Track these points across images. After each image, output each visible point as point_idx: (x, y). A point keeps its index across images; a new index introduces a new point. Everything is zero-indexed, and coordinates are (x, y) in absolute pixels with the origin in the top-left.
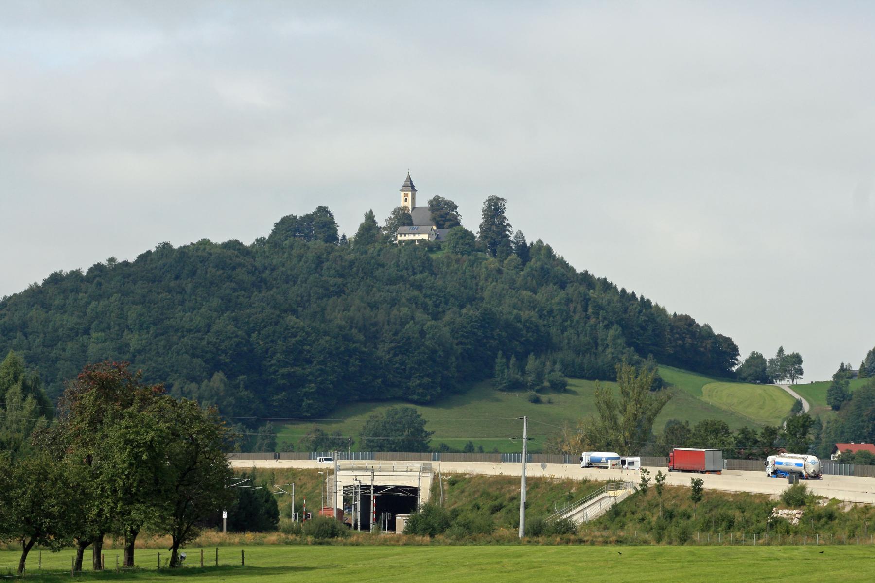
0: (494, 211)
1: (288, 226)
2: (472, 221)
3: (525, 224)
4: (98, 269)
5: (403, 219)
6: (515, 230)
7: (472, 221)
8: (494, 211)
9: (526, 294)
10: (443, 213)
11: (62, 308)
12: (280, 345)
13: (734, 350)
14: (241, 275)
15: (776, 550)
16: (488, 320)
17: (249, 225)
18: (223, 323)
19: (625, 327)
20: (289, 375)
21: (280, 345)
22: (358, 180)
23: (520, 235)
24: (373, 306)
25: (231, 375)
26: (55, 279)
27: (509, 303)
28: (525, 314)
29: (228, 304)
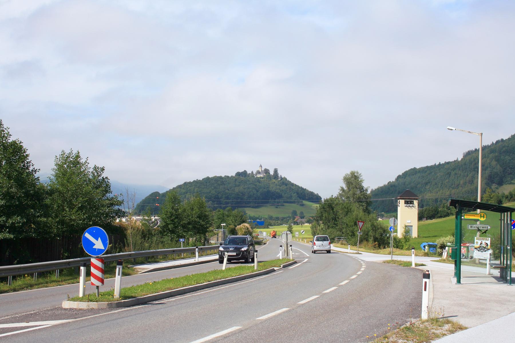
0: (276, 171)
1: (238, 174)
2: (272, 173)
3: (282, 173)
4: (194, 181)
5: (258, 172)
6: (91, 166)
7: (272, 173)
8: (276, 171)
9: (278, 187)
10: (267, 171)
11: (184, 189)
12: (224, 196)
13: (321, 198)
14: (219, 182)
15: (210, 270)
16: (269, 192)
17: (231, 173)
18: (213, 192)
19: (298, 193)
20: (226, 202)
21: (224, 196)
22: (252, 166)
23: (281, 176)
24: (245, 189)
25: (213, 202)
26: (185, 183)
27: (273, 188)
28: (277, 191)
29: (215, 188)
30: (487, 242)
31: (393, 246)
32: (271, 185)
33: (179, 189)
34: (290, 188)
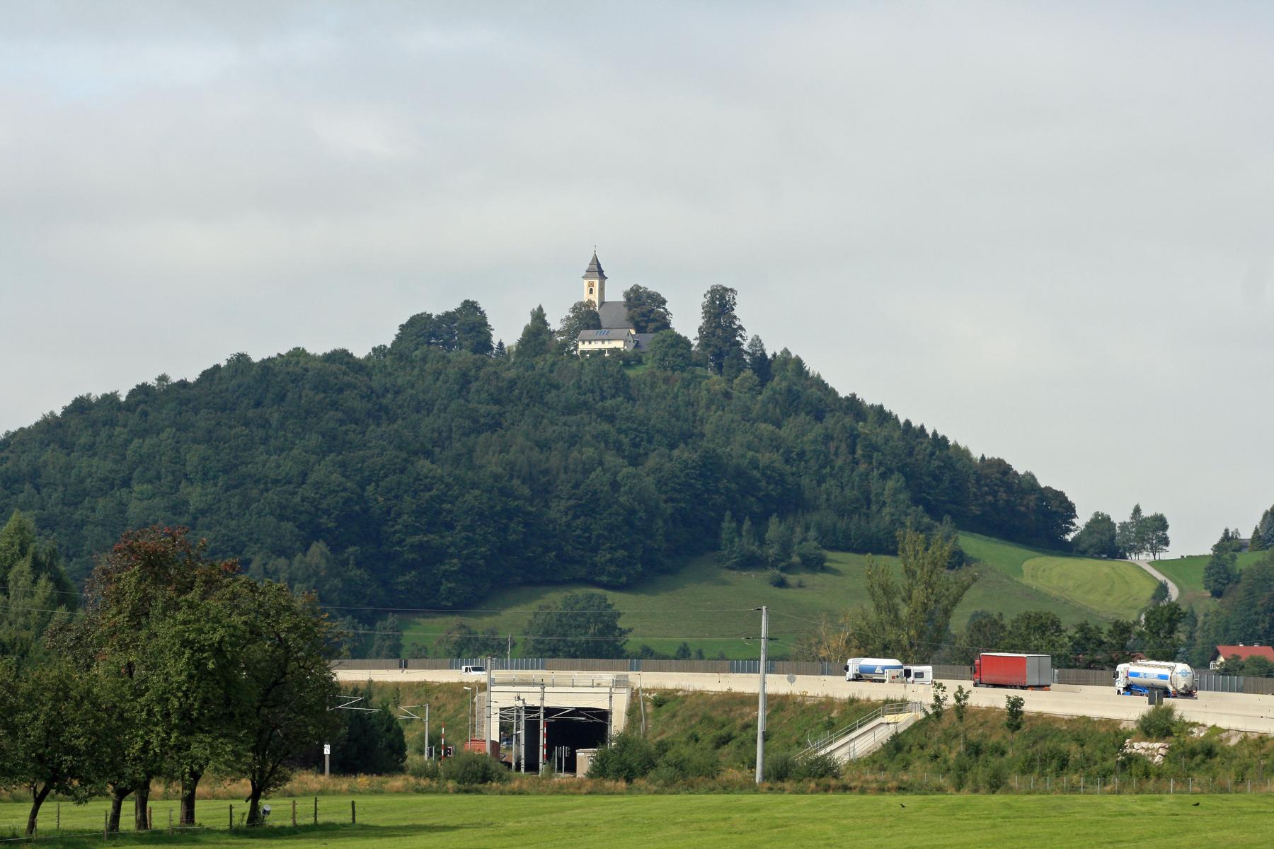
0: (720, 307)
1: (420, 330)
2: (687, 322)
3: (765, 327)
4: (142, 391)
5: (587, 319)
7: (687, 322)
8: (720, 307)
9: (765, 428)
10: (645, 310)
12: (408, 502)
14: (351, 400)
15: (1130, 801)
16: (710, 467)
17: (363, 328)
18: (325, 471)
19: (910, 476)
20: (421, 547)
21: (408, 502)
22: (522, 262)
23: (757, 342)
24: (544, 446)
25: (336, 547)
26: (81, 406)
27: (742, 441)
28: (765, 458)
29: (332, 443)
30: (417, 757)
31: (100, 777)
32: (713, 420)
33: (132, 399)
34: (853, 438)
